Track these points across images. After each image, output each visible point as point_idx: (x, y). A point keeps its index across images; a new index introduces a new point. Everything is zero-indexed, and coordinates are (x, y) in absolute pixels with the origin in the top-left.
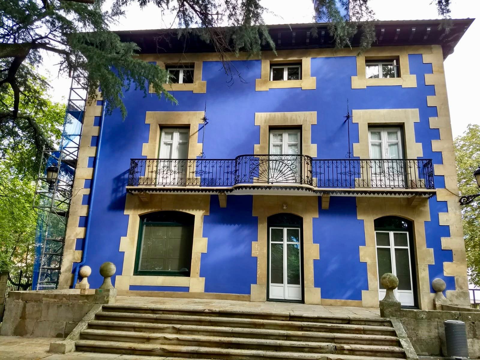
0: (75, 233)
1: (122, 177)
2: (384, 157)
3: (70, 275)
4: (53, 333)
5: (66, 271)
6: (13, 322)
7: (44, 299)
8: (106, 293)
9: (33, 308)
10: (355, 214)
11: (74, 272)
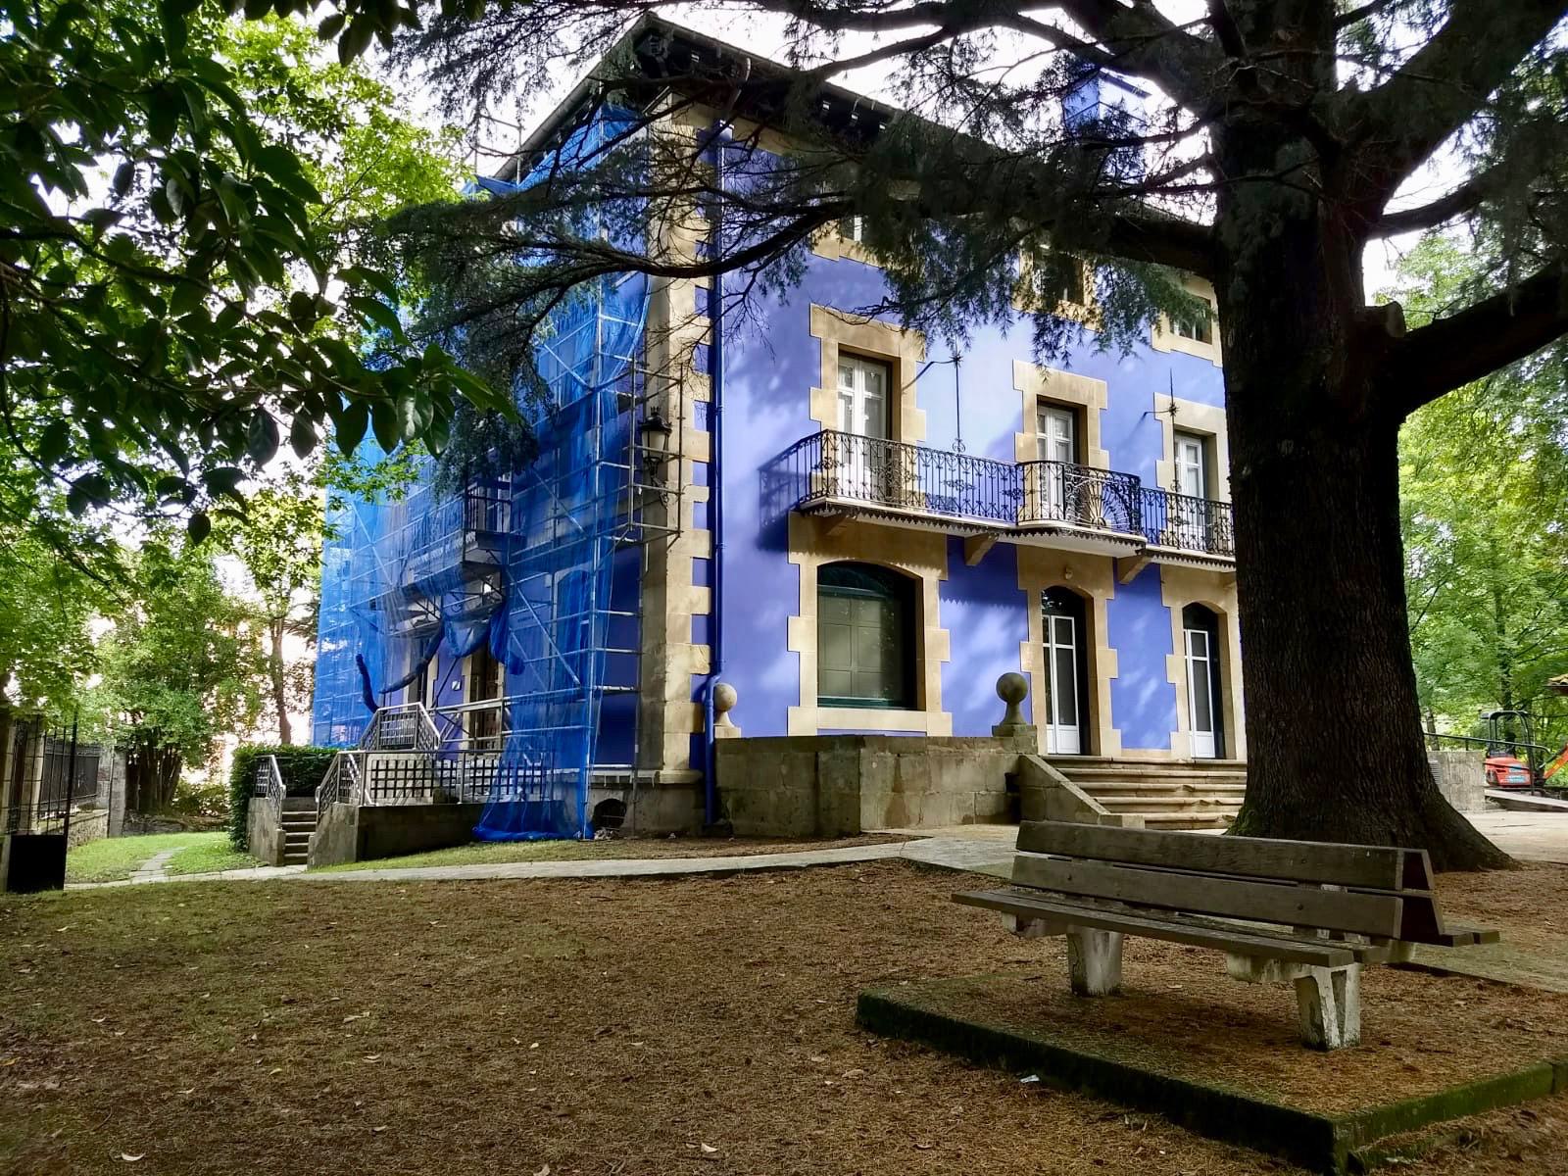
0: (687, 600)
1: (776, 468)
2: (1183, 492)
3: (689, 707)
4: (956, 816)
5: (678, 697)
6: (881, 800)
7: (930, 747)
8: (1032, 733)
9: (914, 767)
10: (1158, 595)
11: (697, 698)
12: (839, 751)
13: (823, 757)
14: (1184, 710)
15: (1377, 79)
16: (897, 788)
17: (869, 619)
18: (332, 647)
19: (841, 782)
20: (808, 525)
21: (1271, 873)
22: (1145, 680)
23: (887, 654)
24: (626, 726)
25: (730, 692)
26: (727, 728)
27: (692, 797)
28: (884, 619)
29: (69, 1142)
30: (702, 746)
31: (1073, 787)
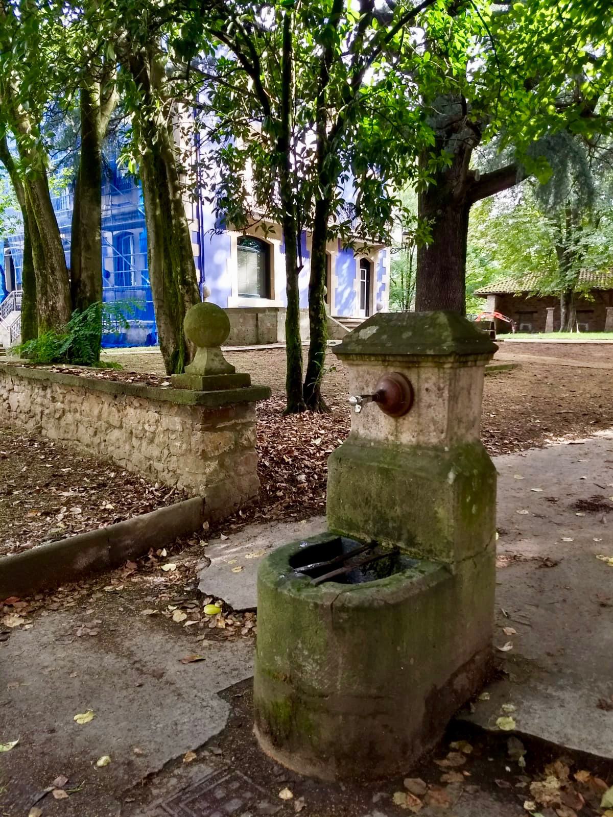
12: (267, 313)
13: (260, 315)
14: (357, 301)
17: (253, 259)
19: (269, 325)
21: (245, 355)
22: (345, 288)
23: (260, 275)
28: (259, 259)
29: (331, 449)
31: (343, 326)
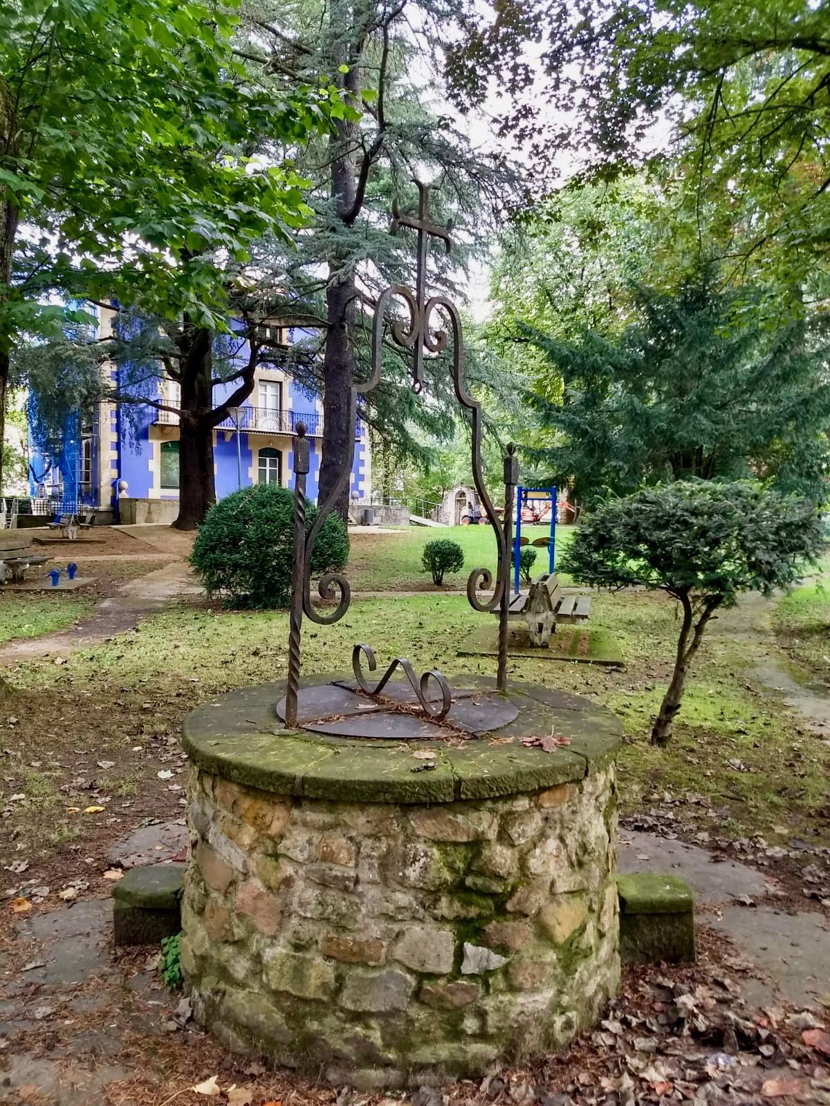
3: (110, 488)
15: (366, 301)
16: (149, 513)
18: (62, 304)
20: (157, 429)
24: (92, 495)
25: (124, 484)
26: (123, 495)
27: (111, 515)
30: (115, 501)
